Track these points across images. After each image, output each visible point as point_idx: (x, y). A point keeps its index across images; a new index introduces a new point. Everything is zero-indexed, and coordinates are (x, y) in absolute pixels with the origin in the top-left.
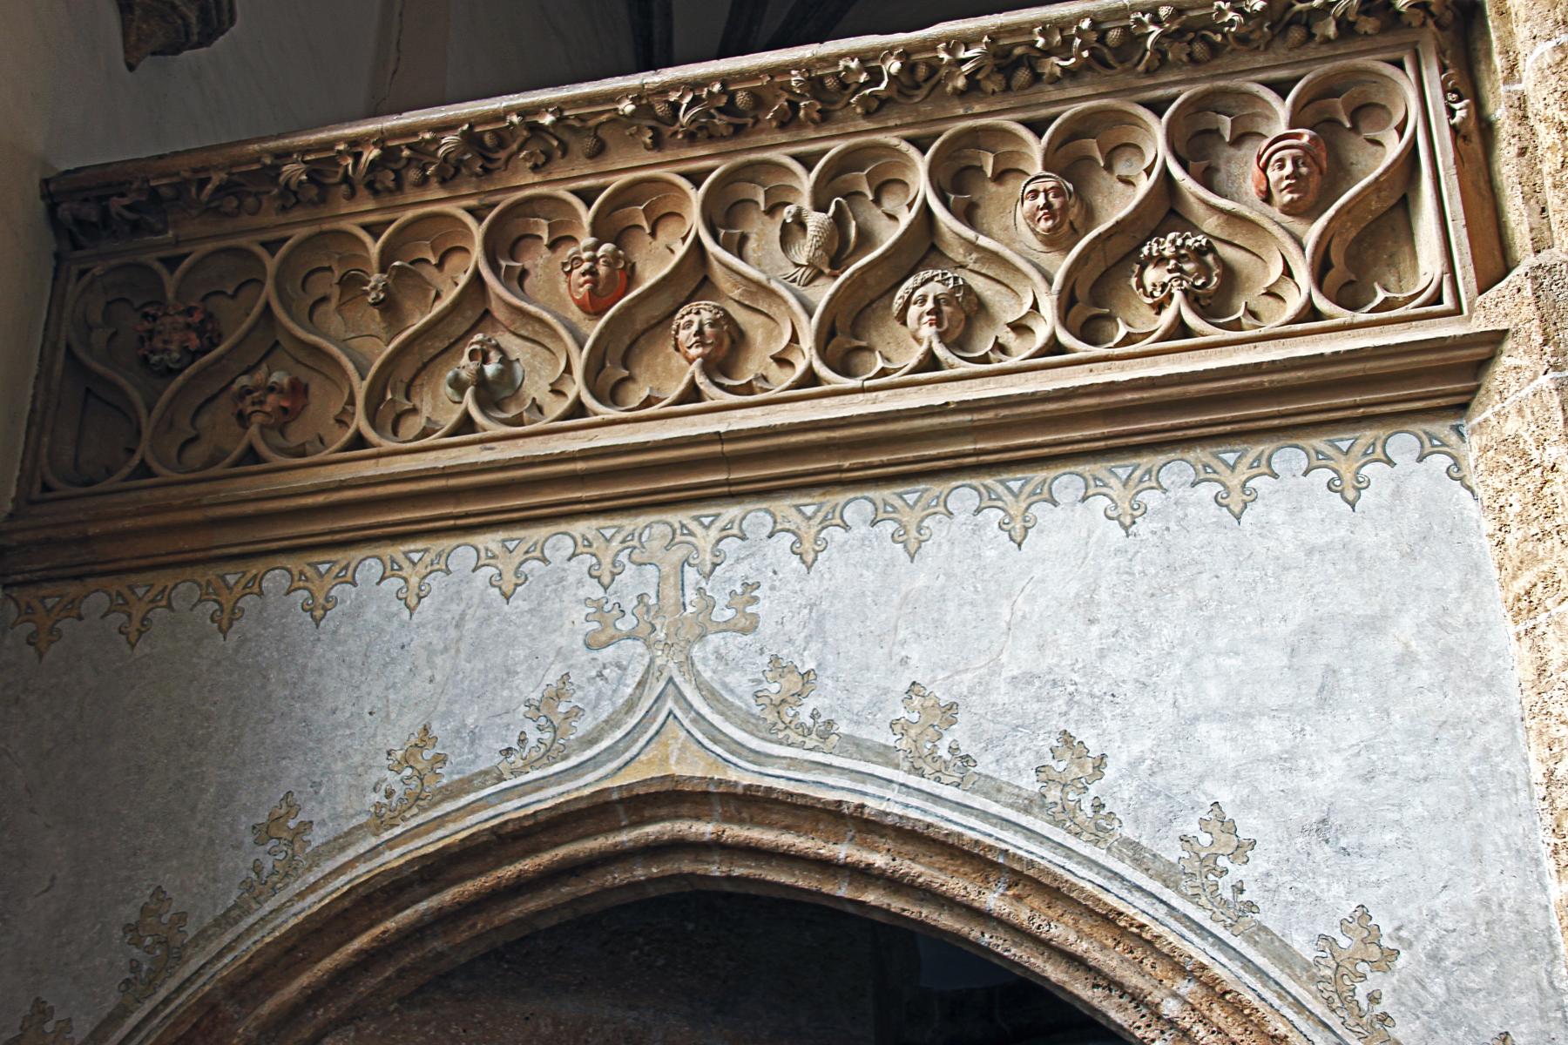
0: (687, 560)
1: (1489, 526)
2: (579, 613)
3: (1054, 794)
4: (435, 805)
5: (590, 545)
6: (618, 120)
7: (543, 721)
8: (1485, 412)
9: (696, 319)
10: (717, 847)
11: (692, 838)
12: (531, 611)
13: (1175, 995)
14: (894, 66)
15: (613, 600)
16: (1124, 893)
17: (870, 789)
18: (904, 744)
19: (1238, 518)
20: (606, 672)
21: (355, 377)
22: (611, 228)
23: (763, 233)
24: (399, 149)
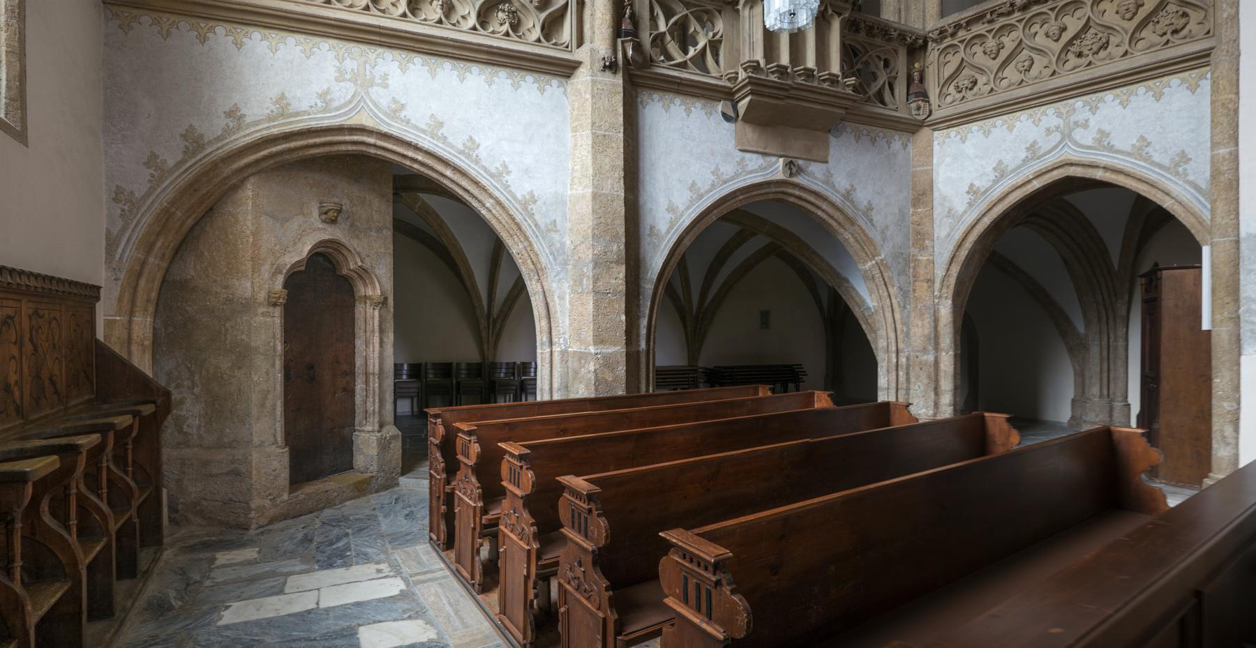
3: (467, 151)
10: (375, 146)
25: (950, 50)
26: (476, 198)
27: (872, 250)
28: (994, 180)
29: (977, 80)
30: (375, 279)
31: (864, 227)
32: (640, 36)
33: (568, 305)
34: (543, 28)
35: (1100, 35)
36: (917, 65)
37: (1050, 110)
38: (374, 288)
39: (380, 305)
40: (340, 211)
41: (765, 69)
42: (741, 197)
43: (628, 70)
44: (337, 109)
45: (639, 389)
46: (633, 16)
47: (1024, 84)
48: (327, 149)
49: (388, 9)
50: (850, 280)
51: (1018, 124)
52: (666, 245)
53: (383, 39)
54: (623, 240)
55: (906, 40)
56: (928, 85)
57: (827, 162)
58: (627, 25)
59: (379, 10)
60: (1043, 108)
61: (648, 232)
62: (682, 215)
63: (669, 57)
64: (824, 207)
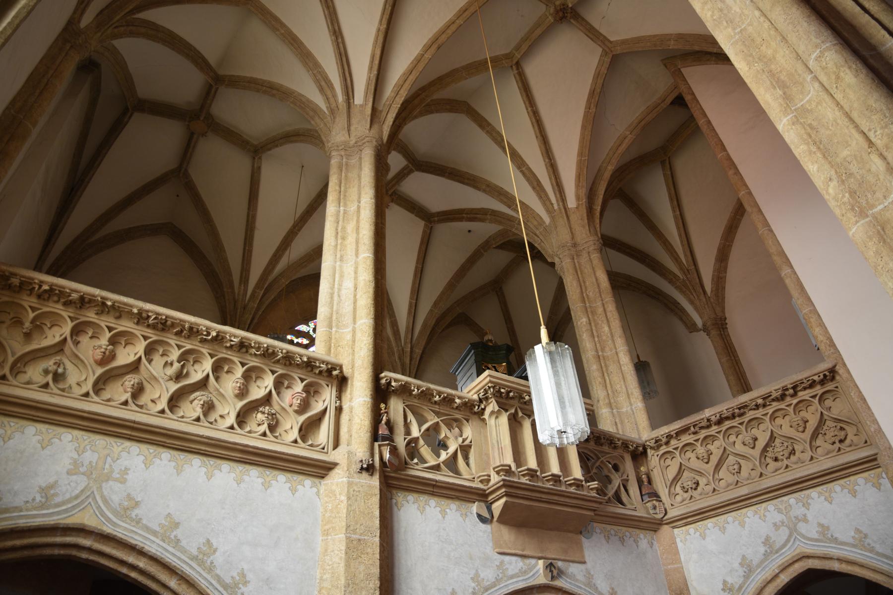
0: (109, 455)
5: (78, 439)
7: (43, 495)
8: (327, 481)
10: (90, 550)
11: (82, 545)
14: (214, 334)
15: (81, 460)
16: (213, 590)
17: (148, 543)
18: (162, 531)
19: (266, 490)
20: (71, 484)
22: (113, 341)
24: (56, 290)
25: (668, 456)
28: (744, 576)
29: (698, 481)
32: (395, 440)
34: (300, 430)
35: (786, 444)
36: (642, 469)
37: (770, 506)
41: (516, 472)
44: (58, 505)
46: (388, 423)
47: (740, 484)
49: (146, 405)
51: (747, 520)
55: (628, 447)
56: (657, 486)
57: (584, 563)
58: (383, 430)
59: (137, 405)
60: (764, 505)
63: (423, 461)
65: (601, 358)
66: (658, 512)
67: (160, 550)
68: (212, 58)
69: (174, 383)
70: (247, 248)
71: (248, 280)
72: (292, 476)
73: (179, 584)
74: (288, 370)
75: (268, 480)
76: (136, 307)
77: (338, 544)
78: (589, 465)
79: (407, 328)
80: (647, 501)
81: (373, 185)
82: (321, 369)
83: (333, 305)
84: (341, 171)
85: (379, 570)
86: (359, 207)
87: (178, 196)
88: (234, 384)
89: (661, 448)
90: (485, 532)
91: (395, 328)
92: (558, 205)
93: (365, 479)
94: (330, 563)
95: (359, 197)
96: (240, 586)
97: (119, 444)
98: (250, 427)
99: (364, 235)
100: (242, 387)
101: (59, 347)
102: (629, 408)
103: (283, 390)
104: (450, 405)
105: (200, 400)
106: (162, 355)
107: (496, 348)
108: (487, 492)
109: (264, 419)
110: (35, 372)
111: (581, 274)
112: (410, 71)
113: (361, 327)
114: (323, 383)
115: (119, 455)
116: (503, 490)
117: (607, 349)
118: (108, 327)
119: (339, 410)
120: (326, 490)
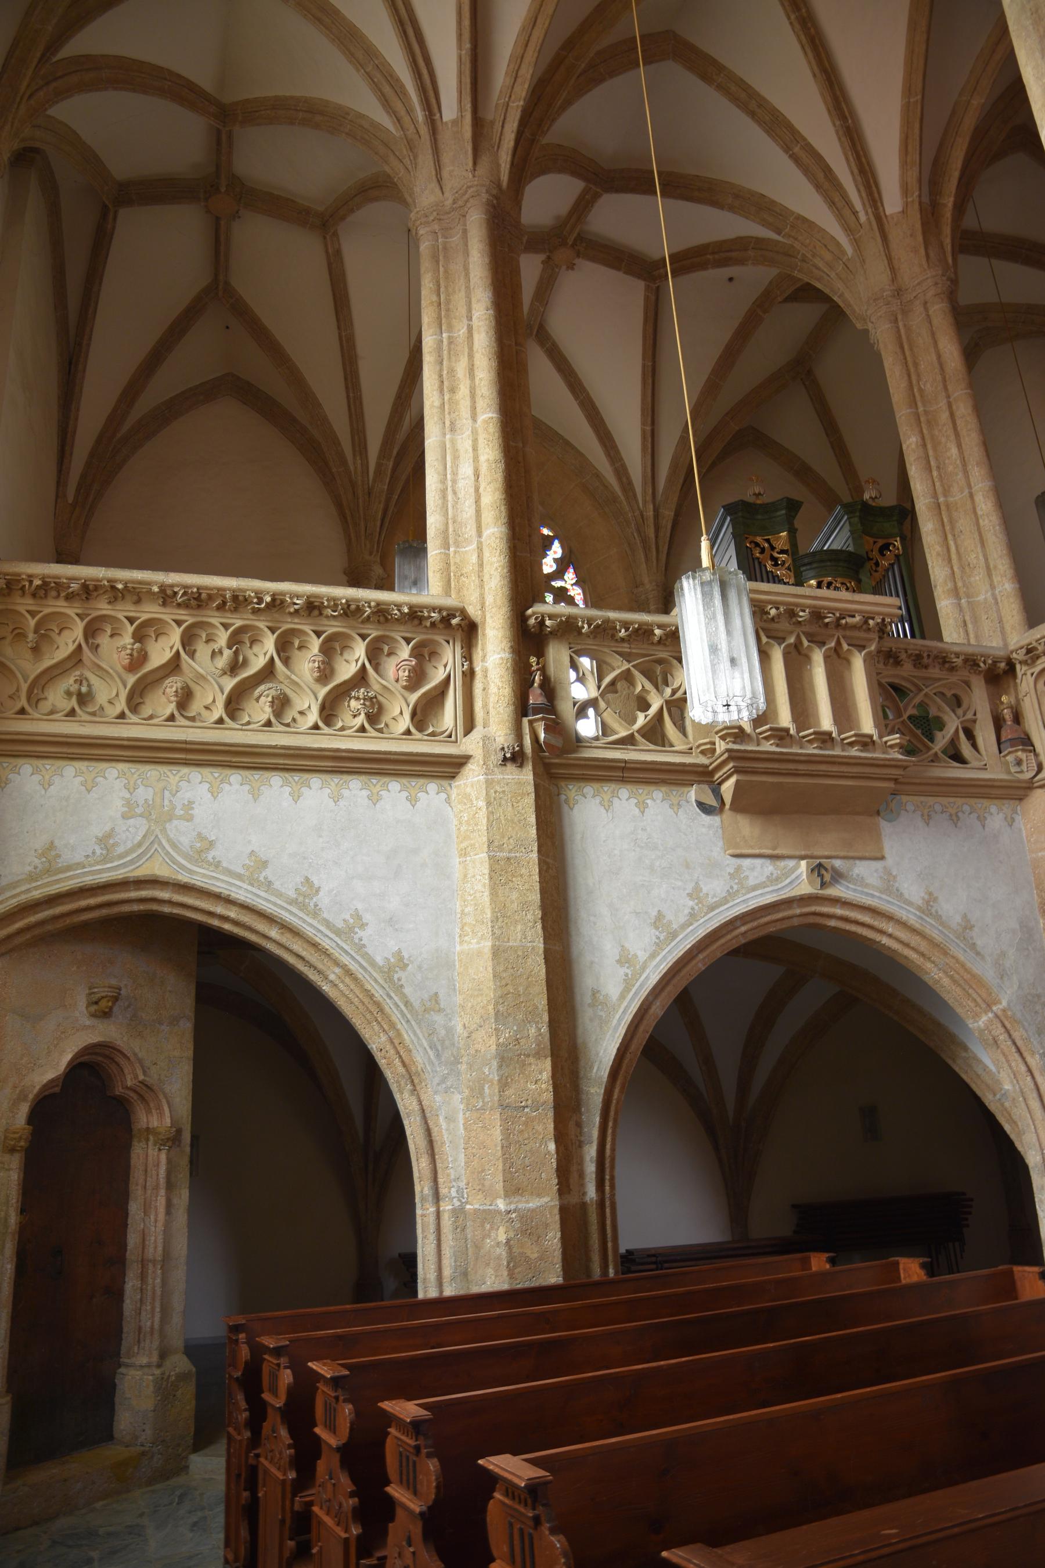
1: (455, 822)
2: (119, 803)
3: (301, 899)
4: (55, 874)
6: (150, 592)
7: (103, 846)
9: (175, 685)
10: (170, 902)
12: (99, 799)
13: (334, 973)
14: (268, 599)
15: (134, 800)
16: (322, 937)
18: (247, 874)
21: (22, 681)
22: (139, 636)
23: (203, 650)
24: (50, 582)
26: (315, 968)
27: (984, 995)
30: (164, 1102)
31: (962, 958)
33: (461, 1130)
34: (414, 715)
36: (1004, 699)
38: (161, 1114)
39: (170, 1143)
40: (116, 999)
42: (743, 929)
43: (542, 758)
44: (121, 856)
45: (588, 1272)
48: (104, 912)
49: (200, 714)
50: (968, 1044)
52: (620, 1020)
53: (189, 757)
54: (546, 1017)
57: (883, 858)
58: (535, 697)
61: (588, 1000)
62: (644, 968)
64: (890, 930)
65: (943, 507)
66: (1025, 770)
67: (249, 896)
68: (205, 81)
69: (229, 678)
70: (351, 395)
71: (365, 448)
72: (409, 782)
73: (282, 933)
74: (385, 630)
75: (375, 791)
76: (156, 583)
77: (479, 865)
78: (901, 705)
79: (644, 476)
80: (1006, 752)
81: (489, 281)
82: (433, 620)
83: (447, 510)
84: (437, 262)
85: (539, 896)
86: (470, 329)
87: (227, 327)
88: (311, 664)
89: (1039, 661)
90: (710, 827)
91: (624, 480)
92: (867, 213)
93: (511, 773)
94: (472, 892)
95: (469, 310)
96: (357, 930)
97: (174, 772)
98: (342, 720)
99: (481, 379)
100: (322, 667)
101: (76, 658)
102: (989, 594)
103: (384, 659)
104: (648, 640)
105: (267, 696)
106: (207, 641)
107: (768, 509)
108: (711, 768)
109: (360, 707)
110: (57, 697)
111: (911, 349)
112: (533, 21)
113: (489, 542)
114: (440, 639)
115: (177, 786)
116: (731, 765)
117: (955, 489)
118: (128, 618)
119: (469, 675)
120: (458, 795)
